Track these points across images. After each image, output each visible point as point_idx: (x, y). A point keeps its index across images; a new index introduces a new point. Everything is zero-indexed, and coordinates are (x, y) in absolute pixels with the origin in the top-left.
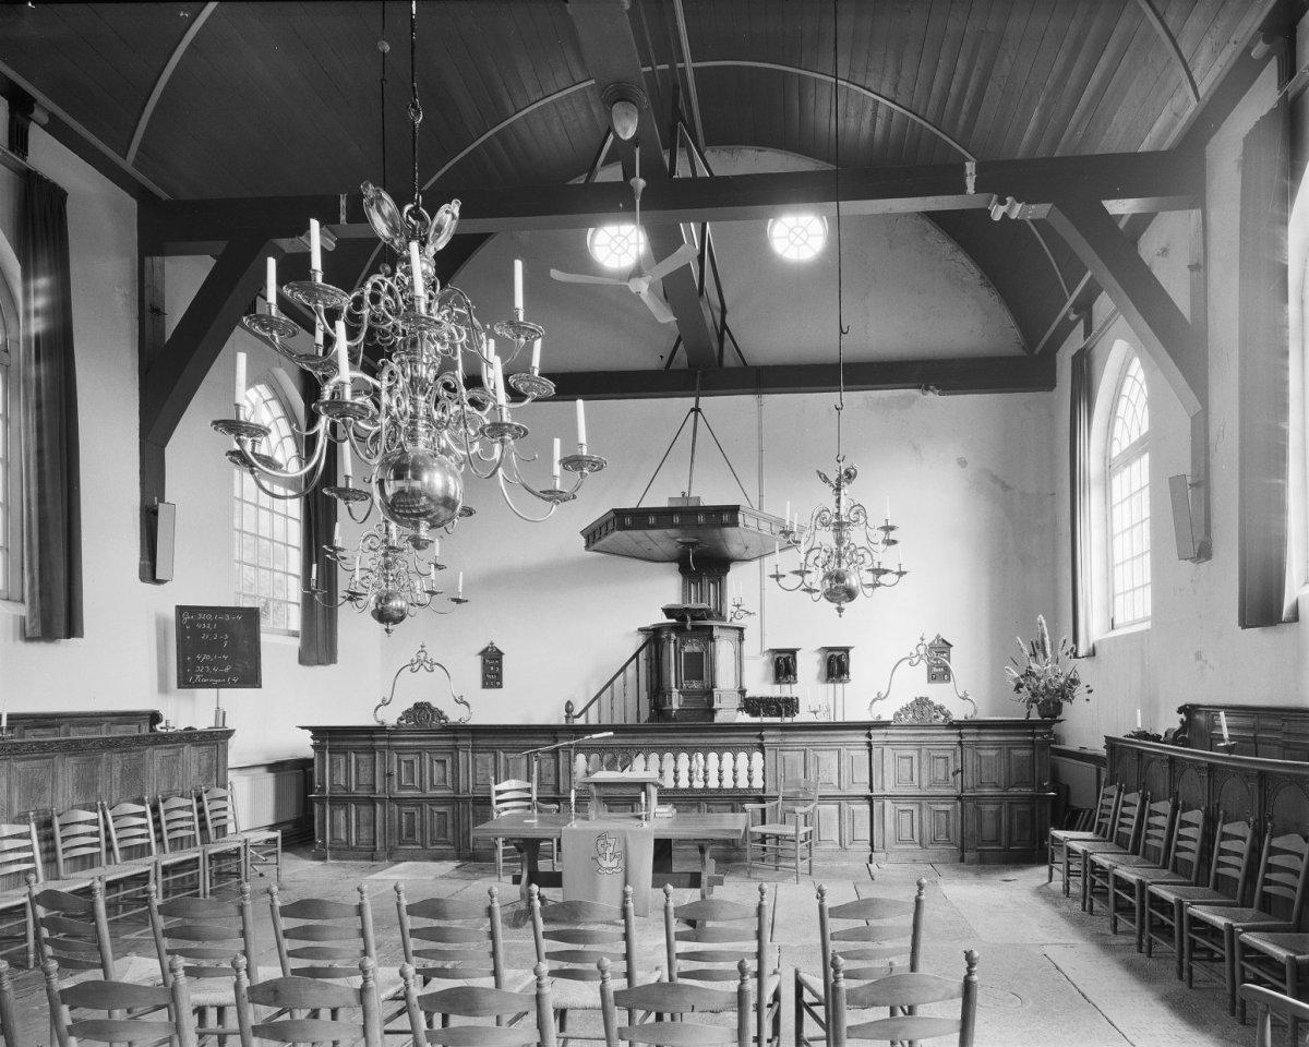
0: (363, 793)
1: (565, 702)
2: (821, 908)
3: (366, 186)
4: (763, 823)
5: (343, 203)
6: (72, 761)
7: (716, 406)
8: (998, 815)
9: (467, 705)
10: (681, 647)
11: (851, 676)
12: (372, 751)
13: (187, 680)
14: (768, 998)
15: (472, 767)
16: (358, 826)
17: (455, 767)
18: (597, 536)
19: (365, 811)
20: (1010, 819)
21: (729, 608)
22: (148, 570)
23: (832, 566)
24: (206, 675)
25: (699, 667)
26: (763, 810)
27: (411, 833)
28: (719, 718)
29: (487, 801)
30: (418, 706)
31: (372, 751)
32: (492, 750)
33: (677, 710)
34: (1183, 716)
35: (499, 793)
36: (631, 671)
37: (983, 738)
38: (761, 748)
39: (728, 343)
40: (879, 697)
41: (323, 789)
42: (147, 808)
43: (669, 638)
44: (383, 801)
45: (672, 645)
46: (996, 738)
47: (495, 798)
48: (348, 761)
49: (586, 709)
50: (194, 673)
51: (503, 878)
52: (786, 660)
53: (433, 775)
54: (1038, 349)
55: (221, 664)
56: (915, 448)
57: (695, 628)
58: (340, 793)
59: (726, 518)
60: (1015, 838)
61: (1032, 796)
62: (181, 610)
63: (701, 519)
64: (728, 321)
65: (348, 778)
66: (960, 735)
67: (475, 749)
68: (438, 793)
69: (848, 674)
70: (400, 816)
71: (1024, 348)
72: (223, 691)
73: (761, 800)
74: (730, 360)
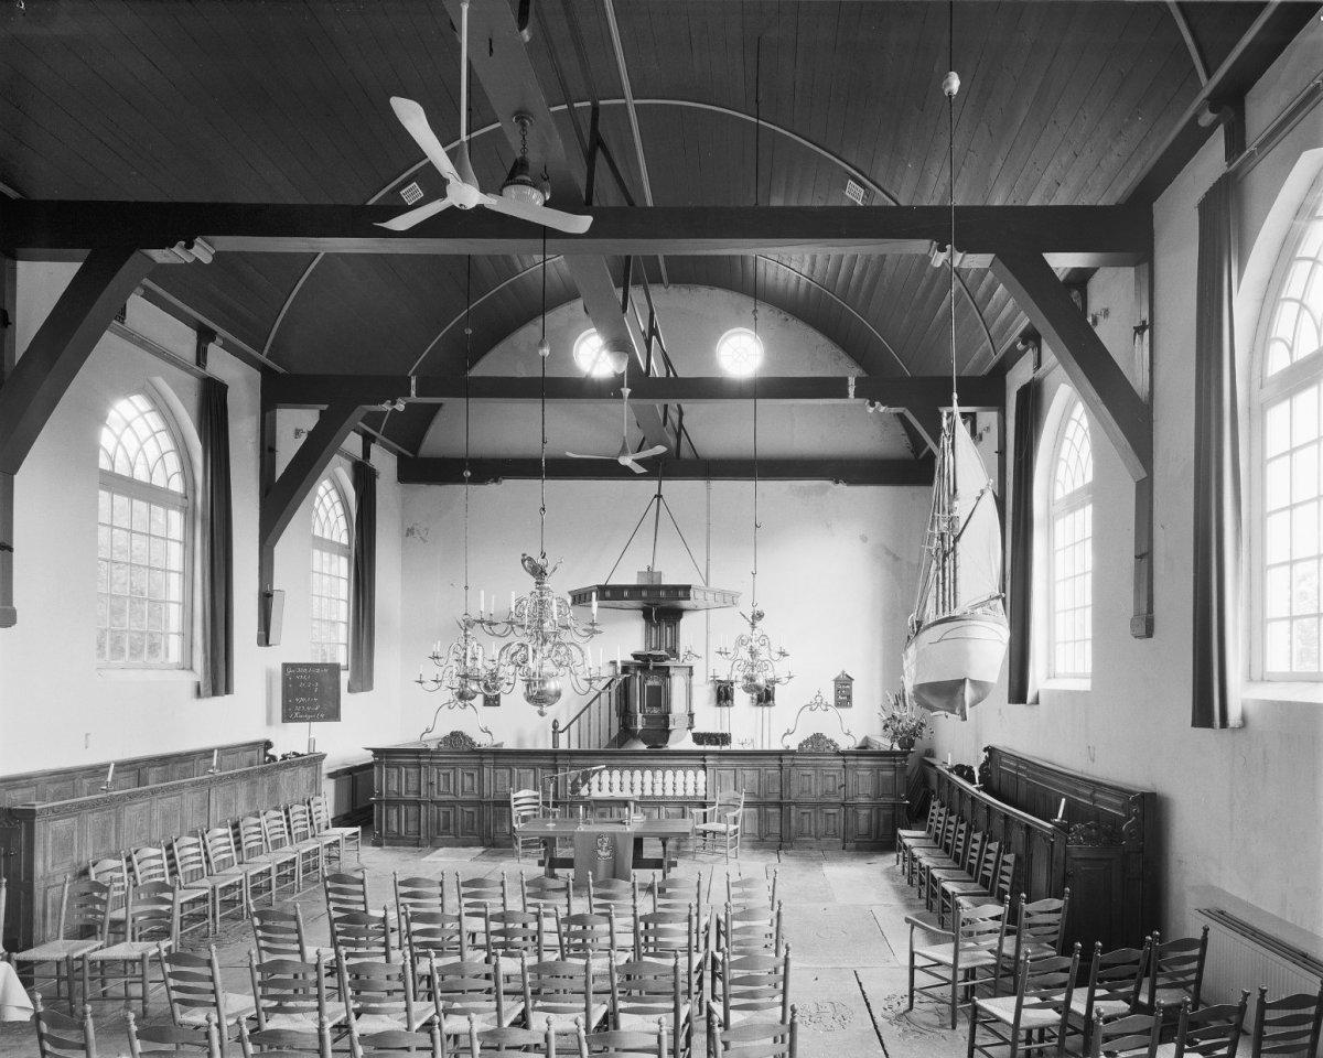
0: (412, 796)
1: (552, 721)
2: (728, 882)
4: (705, 822)
5: (413, 382)
6: (244, 784)
7: (673, 488)
8: (870, 816)
9: (489, 732)
12: (419, 766)
13: (288, 717)
14: (702, 928)
15: (494, 780)
16: (406, 821)
17: (481, 779)
18: (583, 599)
19: (412, 810)
20: (878, 819)
21: (682, 651)
22: (264, 638)
23: (748, 671)
24: (302, 713)
25: (659, 697)
26: (705, 814)
27: (447, 827)
28: (672, 746)
29: (508, 804)
30: (454, 734)
31: (419, 766)
32: (509, 767)
34: (987, 754)
35: (516, 799)
36: (604, 696)
37: (860, 763)
38: (704, 767)
39: (684, 439)
40: (788, 733)
41: (381, 794)
42: (283, 813)
43: (635, 675)
44: (426, 803)
45: (638, 680)
46: (869, 763)
47: (513, 804)
48: (400, 773)
49: (568, 726)
50: (294, 711)
51: (521, 861)
53: (463, 784)
54: (921, 456)
55: (312, 704)
56: (828, 526)
57: (655, 667)
58: (394, 797)
59: (681, 594)
60: (881, 834)
61: (894, 805)
62: (285, 666)
63: (662, 594)
64: (685, 423)
65: (399, 785)
66: (844, 760)
67: (496, 766)
68: (467, 797)
70: (438, 815)
71: (912, 452)
72: (315, 725)
73: (704, 805)
74: (685, 452)
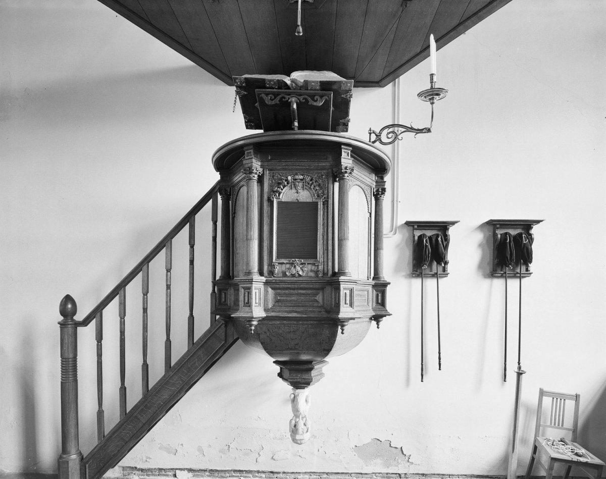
3: (278, 274)
10: (273, 192)
11: (450, 267)
33: (262, 321)
52: (433, 241)
69: (446, 263)
